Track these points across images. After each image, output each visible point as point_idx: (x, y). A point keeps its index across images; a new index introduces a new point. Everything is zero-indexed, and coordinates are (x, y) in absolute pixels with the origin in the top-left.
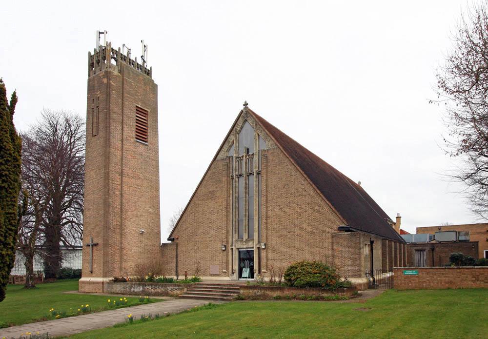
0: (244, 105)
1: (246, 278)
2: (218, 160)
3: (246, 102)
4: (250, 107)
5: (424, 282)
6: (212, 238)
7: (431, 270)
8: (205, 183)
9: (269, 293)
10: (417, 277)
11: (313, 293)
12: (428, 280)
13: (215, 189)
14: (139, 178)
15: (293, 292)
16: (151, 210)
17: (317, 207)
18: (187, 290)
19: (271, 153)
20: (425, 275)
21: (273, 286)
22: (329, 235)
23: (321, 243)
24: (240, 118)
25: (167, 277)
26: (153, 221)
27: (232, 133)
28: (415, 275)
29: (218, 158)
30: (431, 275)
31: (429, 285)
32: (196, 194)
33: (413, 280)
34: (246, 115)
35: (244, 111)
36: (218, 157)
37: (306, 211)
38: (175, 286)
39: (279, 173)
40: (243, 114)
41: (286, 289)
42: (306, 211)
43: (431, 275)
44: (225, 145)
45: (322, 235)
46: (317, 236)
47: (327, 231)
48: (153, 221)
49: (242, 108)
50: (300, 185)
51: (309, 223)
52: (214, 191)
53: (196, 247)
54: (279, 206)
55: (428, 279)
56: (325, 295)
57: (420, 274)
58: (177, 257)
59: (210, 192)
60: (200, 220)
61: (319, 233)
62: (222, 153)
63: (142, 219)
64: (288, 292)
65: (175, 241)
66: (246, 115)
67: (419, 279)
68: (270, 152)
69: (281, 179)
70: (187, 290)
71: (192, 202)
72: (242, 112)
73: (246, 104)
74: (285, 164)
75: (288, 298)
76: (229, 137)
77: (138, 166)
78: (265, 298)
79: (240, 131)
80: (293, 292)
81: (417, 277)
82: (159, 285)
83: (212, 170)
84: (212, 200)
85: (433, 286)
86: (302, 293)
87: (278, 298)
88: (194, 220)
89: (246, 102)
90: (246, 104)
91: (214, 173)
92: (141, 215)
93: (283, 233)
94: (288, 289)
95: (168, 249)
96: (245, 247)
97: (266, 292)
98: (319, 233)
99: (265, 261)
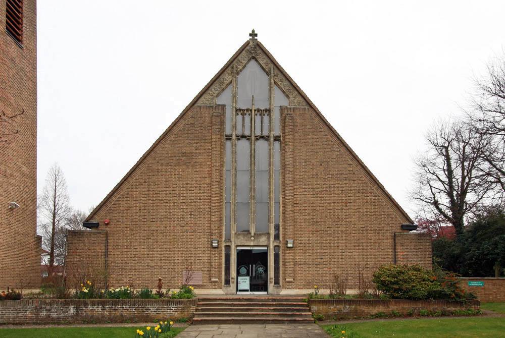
0: (250, 35)
1: (247, 291)
2: (200, 107)
3: (253, 31)
4: (259, 39)
5: (491, 294)
6: (187, 228)
7: (497, 282)
8: (172, 137)
9: (364, 308)
10: (483, 289)
11: (438, 307)
12: (495, 292)
13: (193, 150)
14: (10, 104)
15: (405, 306)
16: (24, 169)
17: (370, 198)
18: (197, 310)
19: (300, 115)
20: (491, 287)
21: (361, 299)
22: (388, 234)
23: (377, 245)
24: (244, 52)
25: (111, 290)
26: (27, 189)
27: (227, 70)
28: (481, 286)
29: (199, 103)
30: (498, 287)
31: (496, 297)
32: (152, 153)
33: (479, 292)
34: (253, 51)
35: (251, 43)
36: (198, 102)
37: (354, 201)
38: (168, 302)
39: (312, 144)
40: (248, 48)
41: (393, 303)
42: (354, 201)
43: (498, 287)
44: (213, 86)
45: (379, 234)
46: (371, 235)
47: (385, 229)
48: (27, 189)
49: (248, 38)
50: (346, 165)
51: (359, 217)
52: (191, 153)
53: (151, 241)
54: (314, 189)
55: (494, 291)
56: (452, 309)
57: (486, 285)
58: (106, 254)
59: (184, 154)
60: (162, 196)
61: (375, 231)
62: (206, 97)
63: (13, 181)
64: (395, 307)
65: (102, 227)
66: (253, 51)
67: (485, 291)
68: (297, 112)
69: (317, 153)
70: (197, 310)
71: (142, 165)
72: (247, 44)
73: (253, 34)
74: (323, 134)
75: (393, 315)
76: (266, 58)
77: (9, 81)
78: (359, 316)
79: (241, 71)
80: (405, 306)
81: (483, 289)
82: (124, 303)
83: (189, 120)
84: (188, 167)
85: (500, 299)
86: (419, 307)
87: (378, 316)
88: (148, 195)
89: (253, 31)
90: (253, 34)
91: (193, 124)
92: (11, 175)
93: (319, 228)
94: (396, 303)
95: (83, 242)
96: (252, 244)
97: (358, 307)
98: (375, 231)
99: (292, 266)
